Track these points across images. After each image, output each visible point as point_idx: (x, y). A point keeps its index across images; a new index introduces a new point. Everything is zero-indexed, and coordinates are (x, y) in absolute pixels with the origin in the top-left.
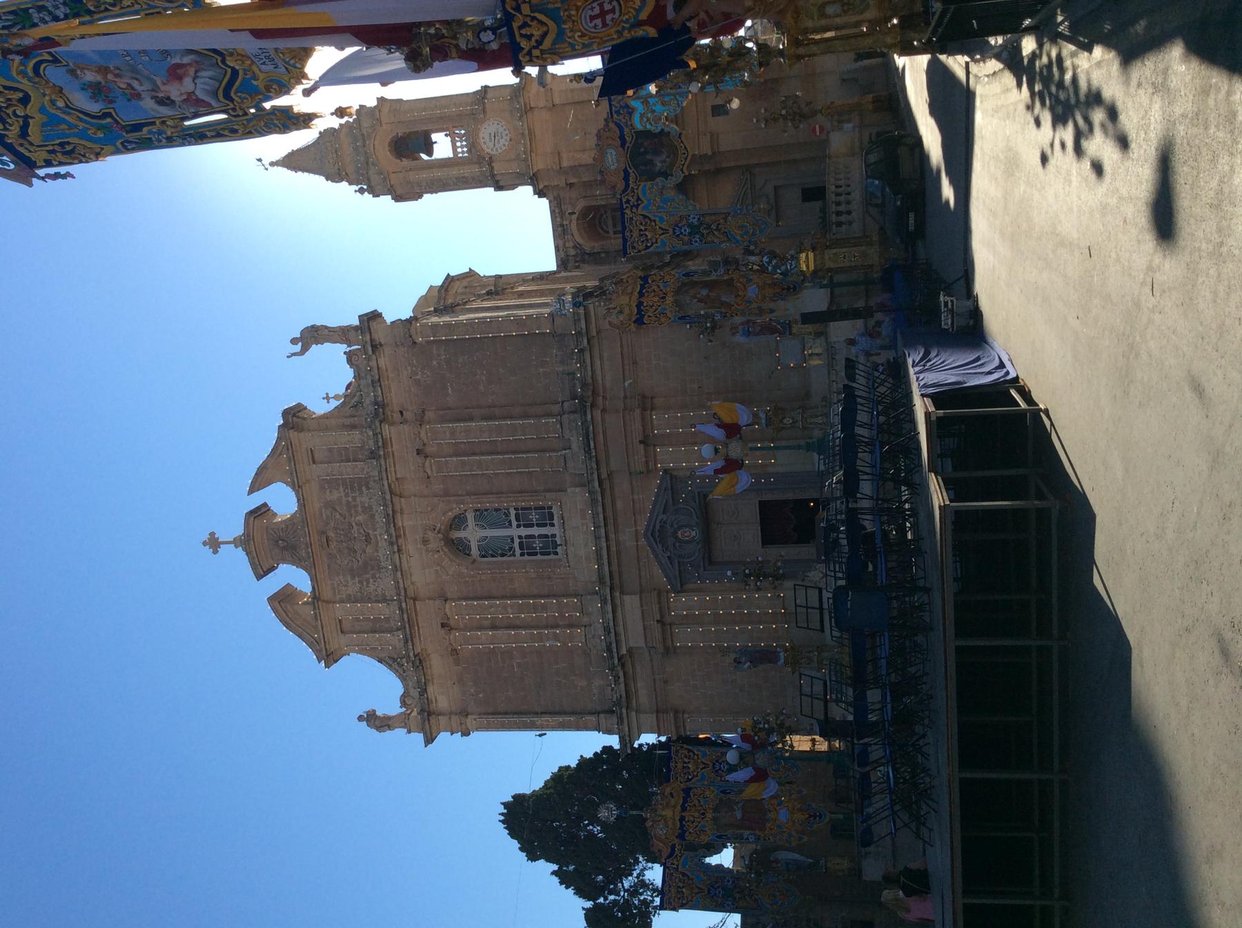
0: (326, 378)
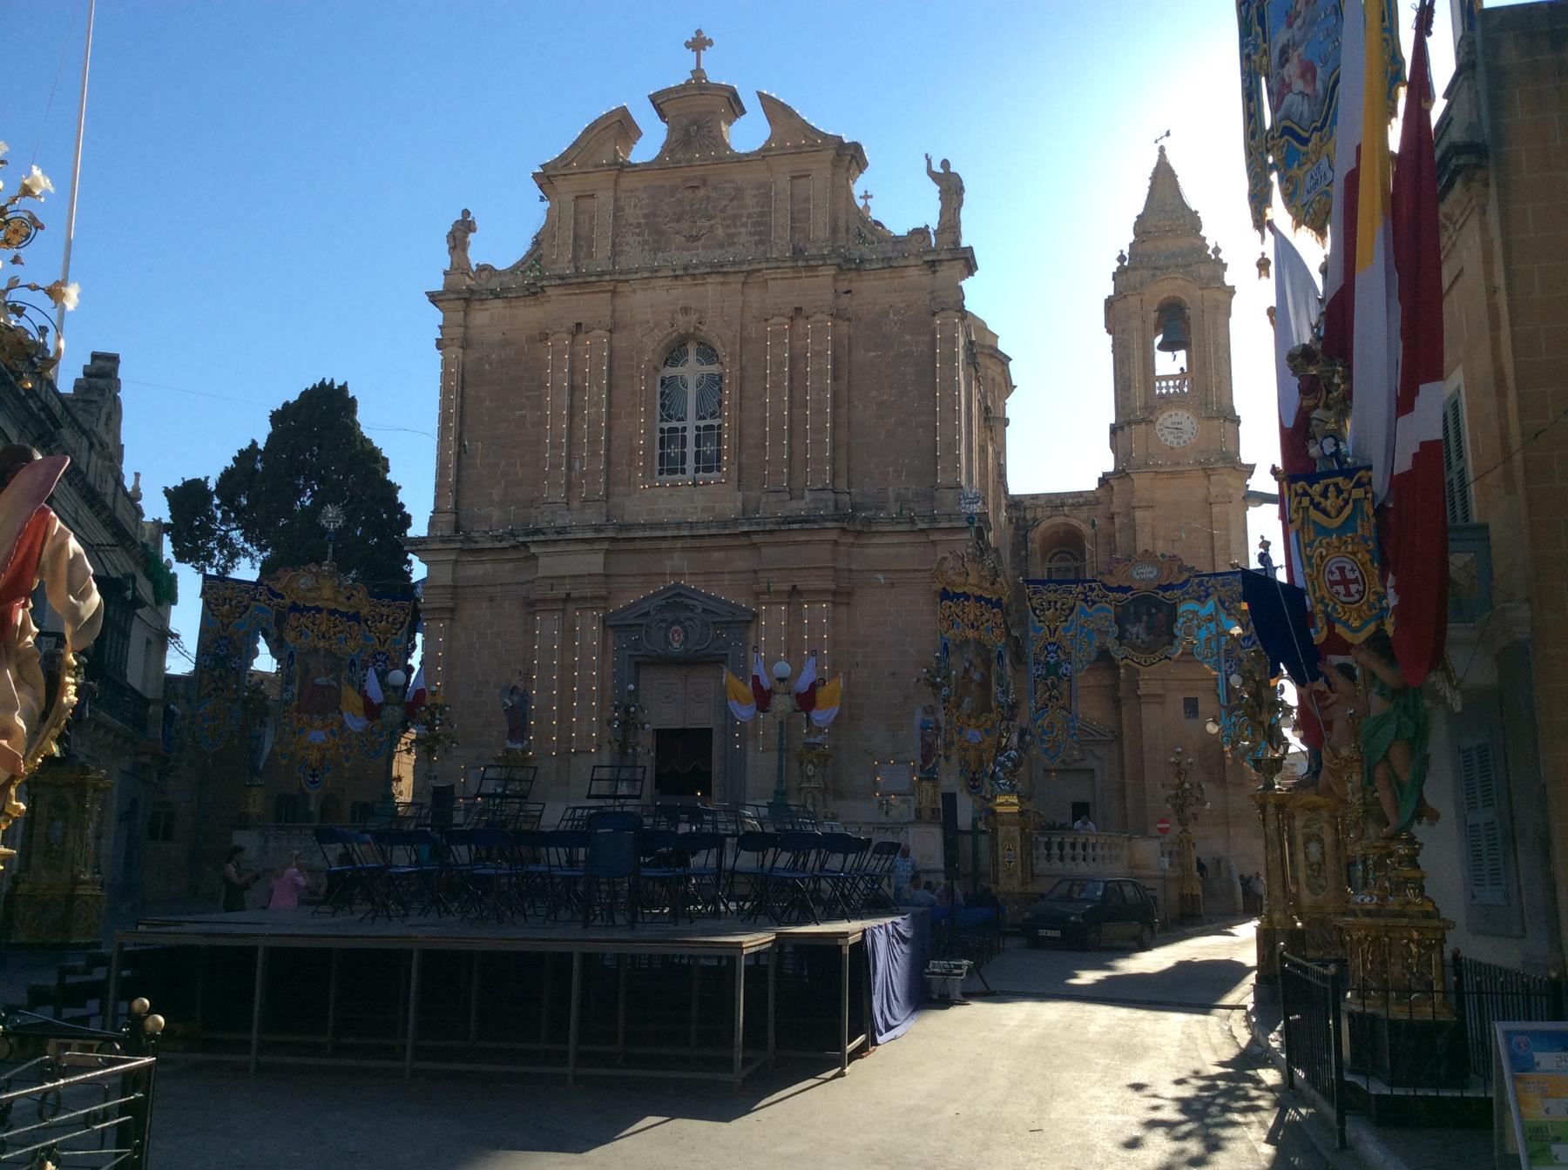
0: (898, 202)
